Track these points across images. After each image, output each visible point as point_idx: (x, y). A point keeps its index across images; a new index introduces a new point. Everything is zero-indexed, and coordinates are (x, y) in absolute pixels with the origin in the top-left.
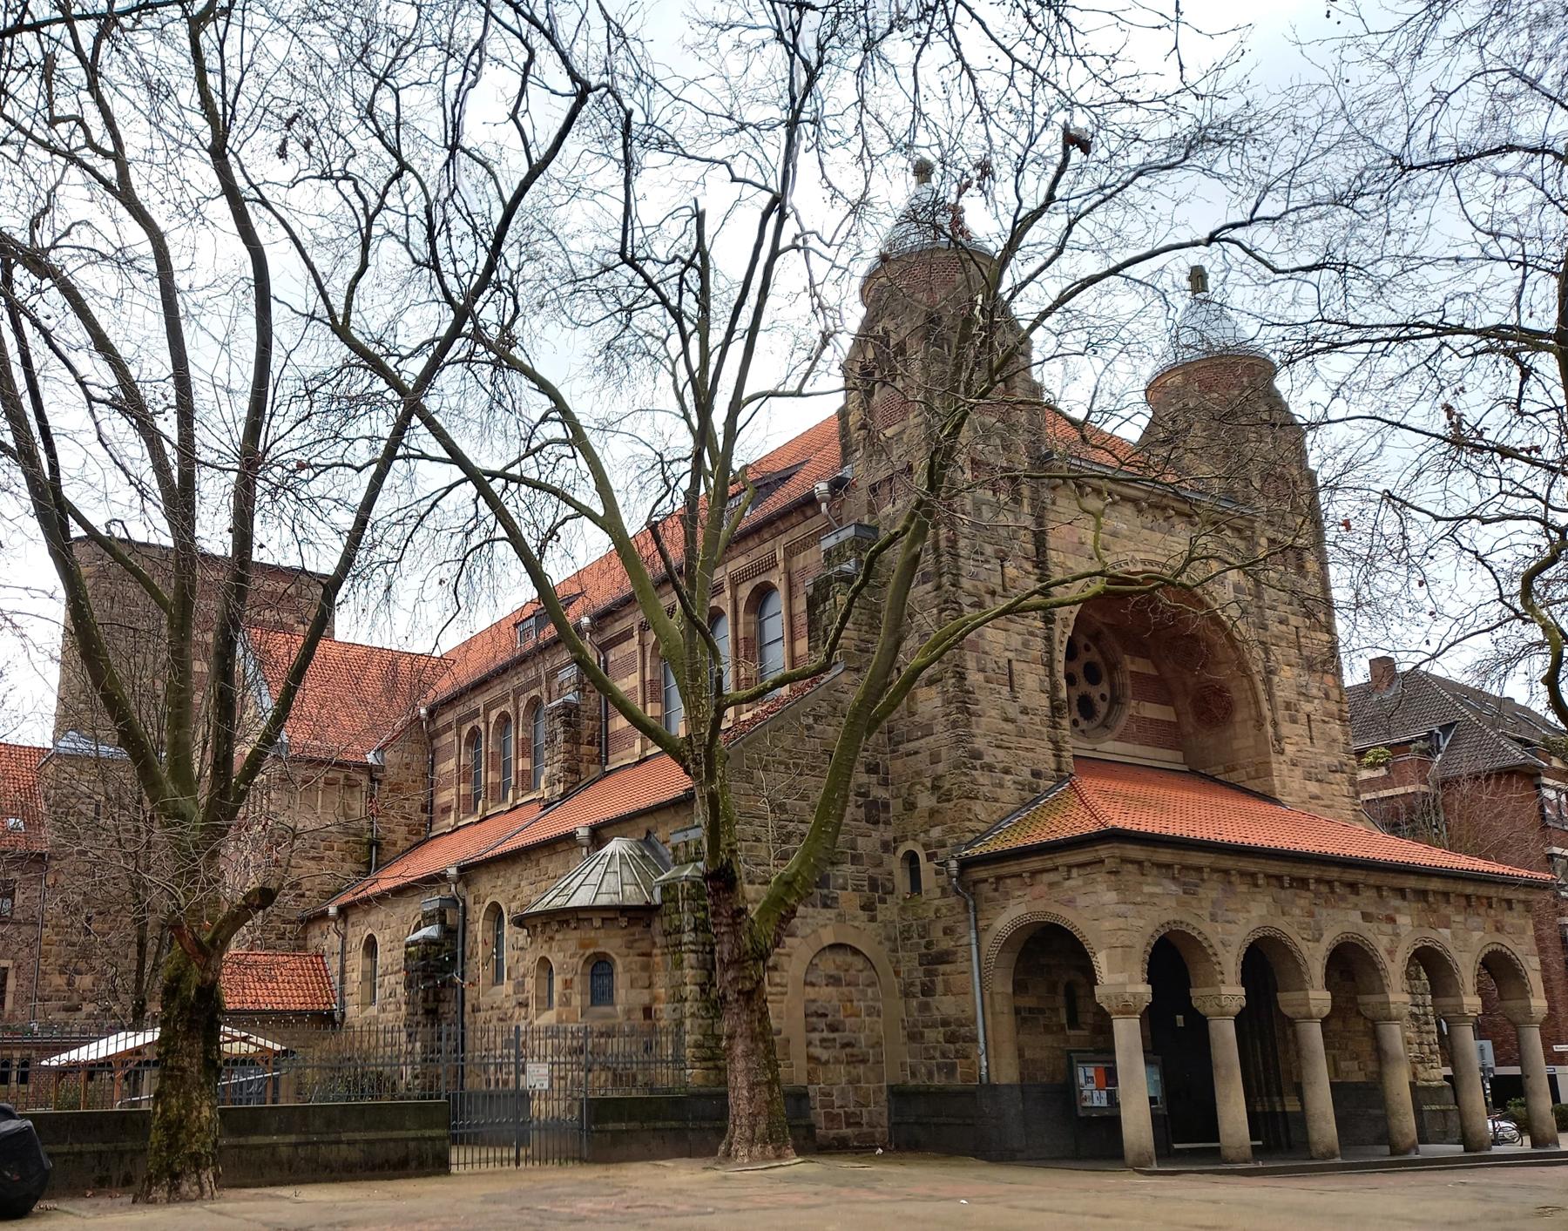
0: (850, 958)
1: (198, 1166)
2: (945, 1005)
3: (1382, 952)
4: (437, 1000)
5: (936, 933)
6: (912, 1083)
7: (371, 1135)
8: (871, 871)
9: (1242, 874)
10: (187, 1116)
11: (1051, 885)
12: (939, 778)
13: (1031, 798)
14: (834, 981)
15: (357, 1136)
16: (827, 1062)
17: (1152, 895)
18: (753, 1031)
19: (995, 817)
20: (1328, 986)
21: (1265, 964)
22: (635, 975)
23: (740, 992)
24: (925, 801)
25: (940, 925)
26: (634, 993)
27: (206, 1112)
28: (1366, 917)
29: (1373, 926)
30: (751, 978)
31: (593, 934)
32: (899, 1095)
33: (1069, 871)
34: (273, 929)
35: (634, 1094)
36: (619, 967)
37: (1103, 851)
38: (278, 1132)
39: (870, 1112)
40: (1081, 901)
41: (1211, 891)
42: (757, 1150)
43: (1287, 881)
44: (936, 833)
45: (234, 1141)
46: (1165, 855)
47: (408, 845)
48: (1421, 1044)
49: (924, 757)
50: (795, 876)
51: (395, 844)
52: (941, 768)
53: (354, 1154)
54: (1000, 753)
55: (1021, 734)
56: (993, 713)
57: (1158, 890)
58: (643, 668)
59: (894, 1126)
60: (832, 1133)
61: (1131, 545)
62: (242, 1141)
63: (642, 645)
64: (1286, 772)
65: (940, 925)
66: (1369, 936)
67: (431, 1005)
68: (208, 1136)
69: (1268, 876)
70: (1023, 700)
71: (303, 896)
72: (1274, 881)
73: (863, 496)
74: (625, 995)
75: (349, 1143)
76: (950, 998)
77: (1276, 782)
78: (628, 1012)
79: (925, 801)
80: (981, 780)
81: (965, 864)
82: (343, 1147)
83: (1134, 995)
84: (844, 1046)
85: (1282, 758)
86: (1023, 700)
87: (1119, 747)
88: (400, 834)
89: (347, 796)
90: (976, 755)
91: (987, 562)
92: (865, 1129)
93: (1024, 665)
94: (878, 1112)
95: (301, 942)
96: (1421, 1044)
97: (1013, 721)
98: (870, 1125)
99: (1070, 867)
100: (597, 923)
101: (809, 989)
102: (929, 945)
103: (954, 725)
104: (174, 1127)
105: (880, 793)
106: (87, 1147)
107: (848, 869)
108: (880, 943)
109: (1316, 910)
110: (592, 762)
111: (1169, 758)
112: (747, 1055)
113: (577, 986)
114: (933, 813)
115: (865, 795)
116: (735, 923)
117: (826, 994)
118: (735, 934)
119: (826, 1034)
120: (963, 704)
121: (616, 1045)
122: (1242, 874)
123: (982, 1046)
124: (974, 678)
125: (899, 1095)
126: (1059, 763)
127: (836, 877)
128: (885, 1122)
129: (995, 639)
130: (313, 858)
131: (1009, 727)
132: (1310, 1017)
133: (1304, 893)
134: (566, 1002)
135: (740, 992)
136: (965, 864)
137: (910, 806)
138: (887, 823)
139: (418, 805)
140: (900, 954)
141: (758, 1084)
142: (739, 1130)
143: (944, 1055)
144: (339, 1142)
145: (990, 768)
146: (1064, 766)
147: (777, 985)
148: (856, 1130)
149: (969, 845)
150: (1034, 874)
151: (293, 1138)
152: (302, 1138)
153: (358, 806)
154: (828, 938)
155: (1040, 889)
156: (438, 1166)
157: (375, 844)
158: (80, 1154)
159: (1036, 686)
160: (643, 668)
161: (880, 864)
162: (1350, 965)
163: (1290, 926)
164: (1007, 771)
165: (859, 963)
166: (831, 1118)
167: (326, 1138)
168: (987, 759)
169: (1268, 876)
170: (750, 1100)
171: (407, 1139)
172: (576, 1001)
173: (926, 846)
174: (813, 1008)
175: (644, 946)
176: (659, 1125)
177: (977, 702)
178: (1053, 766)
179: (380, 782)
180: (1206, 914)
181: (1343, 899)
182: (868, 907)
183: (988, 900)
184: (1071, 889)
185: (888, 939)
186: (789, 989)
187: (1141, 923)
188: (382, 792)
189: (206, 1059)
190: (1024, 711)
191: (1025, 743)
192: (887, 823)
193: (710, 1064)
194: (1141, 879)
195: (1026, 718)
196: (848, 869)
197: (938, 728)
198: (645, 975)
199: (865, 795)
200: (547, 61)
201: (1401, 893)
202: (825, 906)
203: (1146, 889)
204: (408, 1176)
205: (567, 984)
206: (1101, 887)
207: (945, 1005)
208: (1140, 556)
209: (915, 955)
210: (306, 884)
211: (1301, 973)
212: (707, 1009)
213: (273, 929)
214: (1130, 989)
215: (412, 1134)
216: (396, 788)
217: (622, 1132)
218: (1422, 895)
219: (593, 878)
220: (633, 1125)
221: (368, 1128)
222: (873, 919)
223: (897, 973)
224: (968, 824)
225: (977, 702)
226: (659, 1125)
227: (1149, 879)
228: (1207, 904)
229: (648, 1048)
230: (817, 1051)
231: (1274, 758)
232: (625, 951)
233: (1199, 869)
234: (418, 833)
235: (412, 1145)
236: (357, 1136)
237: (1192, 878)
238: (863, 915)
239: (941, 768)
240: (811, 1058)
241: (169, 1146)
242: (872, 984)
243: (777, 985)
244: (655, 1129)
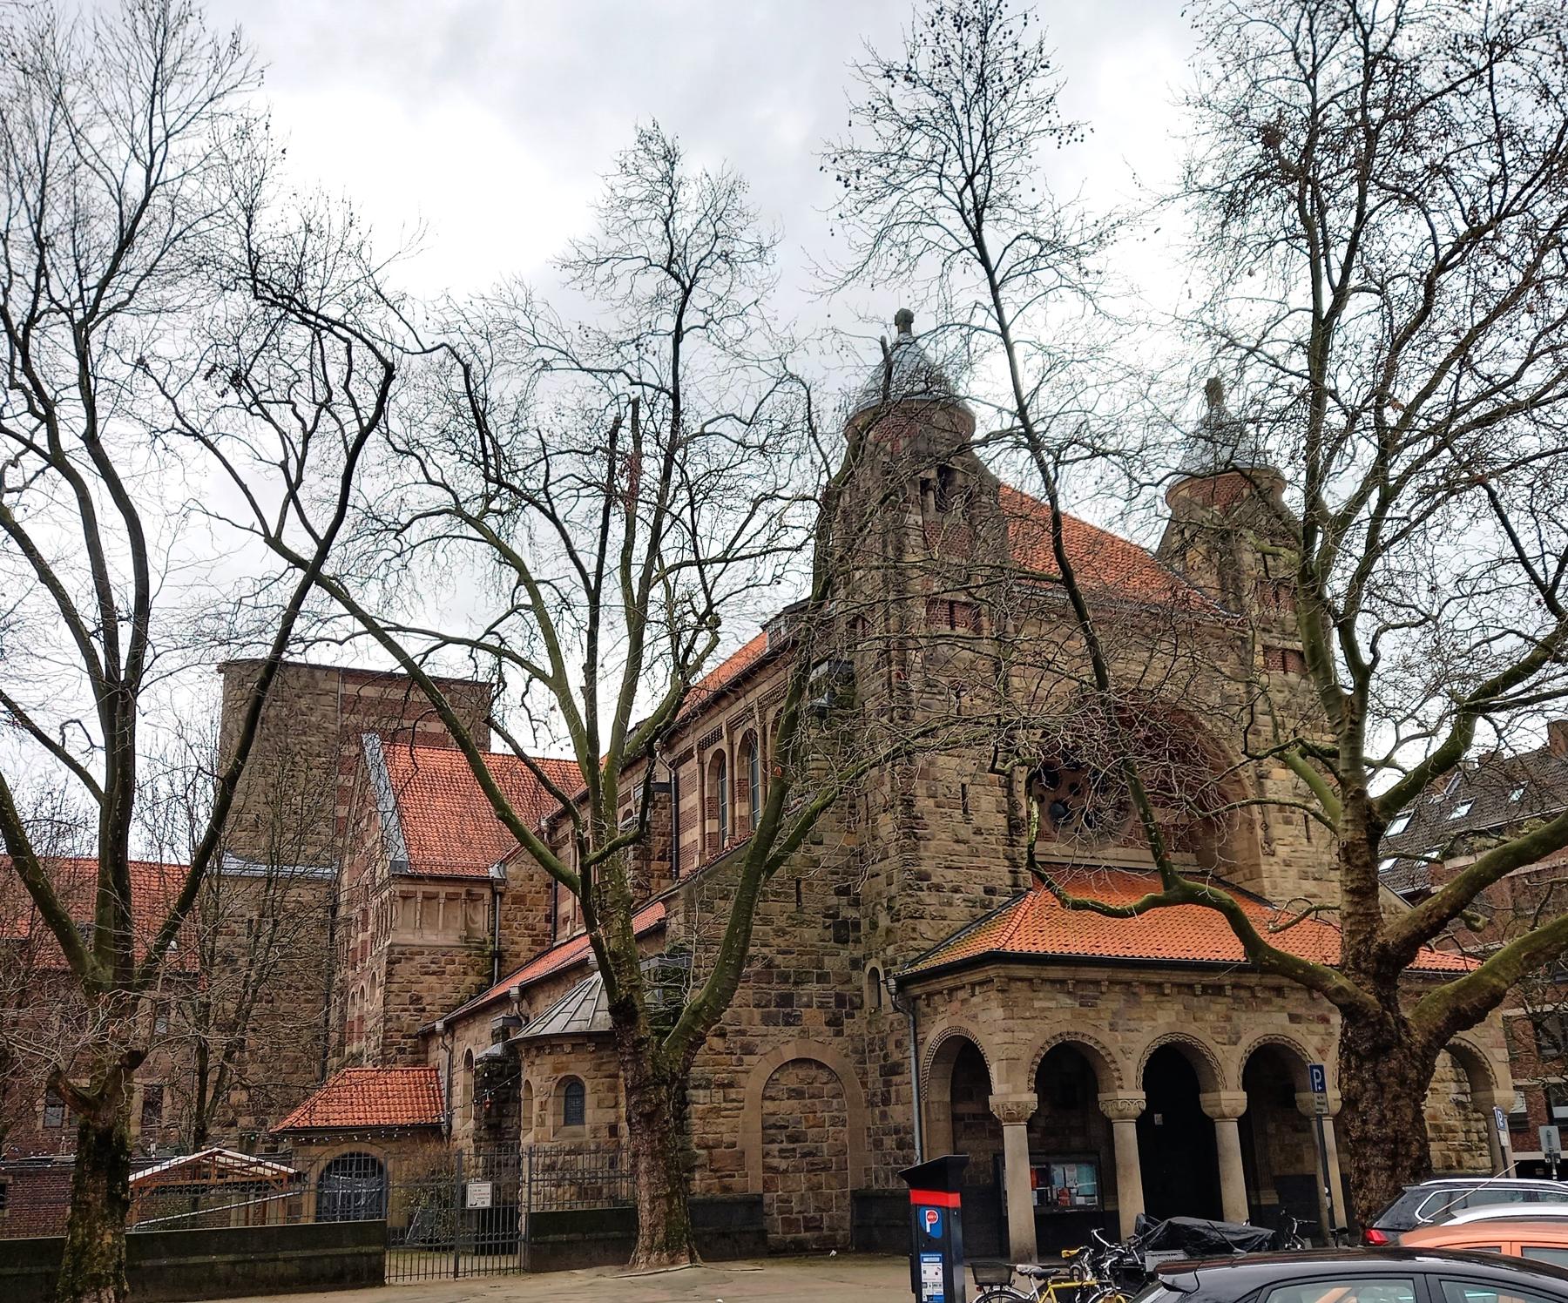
0: (814, 1072)
1: (98, 1286)
2: (897, 1113)
3: (1311, 1051)
4: (501, 1115)
5: (891, 1046)
6: (875, 1187)
7: (308, 1253)
8: (839, 988)
9: (1149, 985)
10: (90, 1243)
11: (964, 1001)
12: (891, 899)
13: (984, 914)
14: (797, 1094)
15: (294, 1254)
16: (786, 1171)
17: (1043, 1010)
18: (653, 1148)
19: (942, 934)
20: (1246, 1086)
21: (1175, 1071)
22: (602, 1095)
23: (641, 1114)
24: (884, 921)
25: (893, 1038)
26: (600, 1112)
27: (108, 1239)
28: (1294, 1018)
29: (1302, 1027)
30: (650, 1100)
31: (564, 1058)
32: (862, 1199)
33: (973, 989)
34: (393, 1044)
35: (599, 1206)
36: (588, 1085)
37: (991, 971)
38: (217, 1252)
39: (831, 1217)
40: (982, 1017)
41: (1112, 1003)
42: (654, 1257)
43: (1198, 989)
44: (890, 950)
45: (173, 1261)
46: (1056, 972)
47: (532, 955)
48: (1468, 1132)
49: (882, 878)
50: (701, 1005)
51: (518, 956)
52: (894, 889)
53: (292, 1270)
54: (950, 874)
55: (975, 853)
56: (944, 836)
57: (1052, 1004)
58: (703, 785)
59: (856, 1228)
60: (789, 1237)
62: (182, 1261)
63: (702, 764)
64: (1277, 873)
65: (893, 1038)
66: (1297, 1037)
67: (493, 1121)
68: (110, 1259)
69: (1174, 985)
70: (977, 820)
71: (423, 1010)
73: (843, 627)
74: (594, 1115)
75: (285, 1260)
76: (900, 1108)
77: (1266, 883)
78: (595, 1130)
79: (884, 921)
80: (928, 900)
81: (903, 983)
82: (279, 1264)
83: (1018, 1104)
84: (804, 1155)
85: (1273, 860)
86: (977, 820)
87: (1121, 852)
88: (523, 945)
89: (470, 911)
90: (924, 877)
91: (941, 693)
92: (826, 1232)
93: (980, 789)
94: (841, 1215)
95: (422, 1056)
96: (1468, 1132)
97: (965, 842)
98: (830, 1229)
99: (973, 985)
100: (568, 1049)
101: (767, 1103)
102: (886, 1057)
103: (902, 849)
104: (81, 1251)
105: (852, 914)
106: (35, 1270)
107: (813, 987)
108: (846, 1056)
109: (1234, 1014)
110: (664, 877)
112: (648, 1172)
113: (550, 1108)
114: (889, 931)
115: (835, 916)
116: (636, 1052)
117: (786, 1107)
118: (636, 1061)
119: (785, 1145)
120: (912, 828)
121: (582, 1162)
122: (1149, 985)
123: (918, 1152)
124: (923, 804)
125: (862, 1199)
126: (1015, 879)
127: (800, 996)
128: (847, 1226)
129: (950, 768)
130: (434, 973)
131: (961, 847)
132: (1223, 1117)
133: (1220, 1000)
134: (542, 1124)
135: (641, 1114)
136: (903, 983)
137: (874, 926)
138: (857, 941)
139: (542, 915)
140: (868, 1065)
141: (658, 1197)
142: (643, 1241)
143: (896, 1162)
144: (276, 1259)
145: (938, 888)
146: (1021, 882)
147: (733, 1101)
148: (816, 1234)
149: (914, 962)
150: (952, 991)
151: (231, 1257)
152: (241, 1257)
153: (481, 919)
154: (790, 1053)
155: (956, 1005)
156: (373, 1277)
157: (499, 955)
158: (30, 1275)
159: (993, 807)
160: (703, 785)
161: (849, 981)
162: (1175, 1071)
164: (956, 890)
165: (824, 1076)
166: (789, 1223)
167: (262, 1256)
168: (934, 880)
169: (1174, 985)
170: (651, 1211)
171: (343, 1256)
172: (550, 1121)
173: (884, 964)
174: (772, 1120)
175: (612, 1068)
176: (601, 1235)
177: (926, 826)
178: (1009, 882)
179: (502, 895)
180: (1105, 1025)
181: (1268, 1002)
182: (835, 1023)
183: (925, 1015)
184: (975, 1006)
185: (855, 1051)
186: (746, 1104)
187: (1030, 1036)
188: (505, 907)
189: (109, 1194)
190: (978, 832)
191: (976, 862)
192: (857, 941)
194: (1031, 995)
195: (979, 838)
196: (813, 987)
197: (892, 852)
198: (611, 1095)
199: (835, 916)
200: (359, 350)
202: (787, 1024)
203: (1037, 1004)
204: (343, 1289)
205: (543, 1106)
206: (994, 1004)
207: (897, 1113)
209: (877, 1066)
210: (428, 1000)
211: (1214, 1076)
213: (393, 1044)
214: (1014, 1098)
215: (348, 1251)
216: (519, 899)
217: (561, 1242)
219: (572, 1006)
220: (578, 1236)
221: (305, 1247)
222: (839, 1033)
223: (864, 1084)
224: (911, 943)
225: (926, 826)
227: (1041, 995)
228: (1108, 1015)
229: (613, 1164)
230: (775, 1162)
231: (1263, 860)
232: (593, 1074)
233: (1097, 983)
234: (543, 943)
235: (348, 1260)
236: (294, 1254)
237: (1090, 991)
238: (829, 1031)
239: (894, 889)
240: (768, 1168)
241: (74, 1269)
242: (838, 1095)
243: (733, 1101)
244: (597, 1240)
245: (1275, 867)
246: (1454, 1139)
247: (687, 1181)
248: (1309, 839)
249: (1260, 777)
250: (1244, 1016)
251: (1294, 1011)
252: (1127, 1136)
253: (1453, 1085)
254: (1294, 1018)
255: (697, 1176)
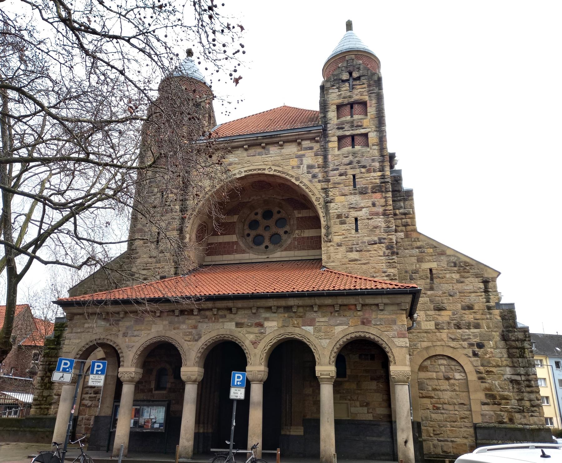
28: (238, 325)
29: (244, 330)
56: (145, 256)
61: (240, 166)
72: (171, 313)
85: (329, 244)
87: (284, 254)
109: (200, 325)
111: (306, 254)
119: (93, 395)
133: (193, 317)
163: (307, 332)
176: (10, 429)
181: (225, 316)
191: (158, 265)
193: (38, 407)
194: (83, 321)
201: (269, 309)
208: (243, 170)
212: (42, 386)
218: (288, 309)
226: (10, 429)
245: (332, 248)
246: (507, 404)
247: (48, 409)
248: (357, 230)
249: (327, 202)
250: (205, 325)
251: (240, 321)
252: (191, 392)
253: (508, 369)
254: (238, 325)
255: (52, 407)
